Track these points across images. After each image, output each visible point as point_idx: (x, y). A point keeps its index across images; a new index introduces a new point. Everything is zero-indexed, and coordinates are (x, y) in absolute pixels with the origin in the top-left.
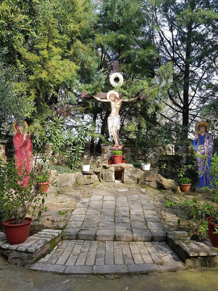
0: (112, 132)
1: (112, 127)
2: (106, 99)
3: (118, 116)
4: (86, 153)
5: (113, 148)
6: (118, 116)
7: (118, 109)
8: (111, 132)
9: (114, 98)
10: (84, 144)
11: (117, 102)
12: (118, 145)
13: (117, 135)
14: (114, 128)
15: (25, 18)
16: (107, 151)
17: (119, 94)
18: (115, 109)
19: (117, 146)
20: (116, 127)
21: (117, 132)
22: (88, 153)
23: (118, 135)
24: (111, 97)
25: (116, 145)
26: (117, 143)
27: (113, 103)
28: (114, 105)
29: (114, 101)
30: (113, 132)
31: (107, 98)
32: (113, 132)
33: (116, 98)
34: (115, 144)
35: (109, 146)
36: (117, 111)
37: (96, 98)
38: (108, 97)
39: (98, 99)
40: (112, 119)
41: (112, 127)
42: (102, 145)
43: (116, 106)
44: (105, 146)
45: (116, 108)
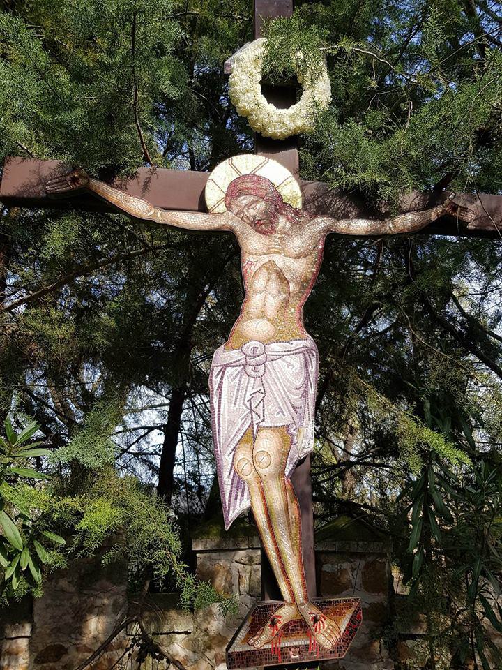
0: (249, 477)
1: (250, 437)
2: (203, 208)
3: (297, 344)
4: (98, 602)
5: (262, 641)
6: (297, 344)
7: (293, 287)
8: (239, 483)
9: (261, 206)
10: (37, 575)
11: (287, 235)
12: (310, 612)
13: (293, 507)
14: (268, 444)
15: (244, 483)
16: (231, 585)
17: (302, 188)
18: (274, 286)
19: (299, 626)
20: (286, 436)
21: (294, 474)
22: (115, 602)
23: (303, 508)
24: (244, 201)
25: (285, 614)
26: (300, 597)
27: (252, 243)
28: (266, 258)
29: (264, 225)
30: (260, 479)
31: (210, 202)
32: (260, 479)
33: (277, 205)
34: (278, 595)
35: (242, 553)
36: (286, 302)
37: (116, 196)
38: (213, 196)
39: (138, 207)
40: (250, 366)
41: (250, 437)
42: (200, 548)
43: (280, 261)
44: (214, 555)
45: (280, 276)
